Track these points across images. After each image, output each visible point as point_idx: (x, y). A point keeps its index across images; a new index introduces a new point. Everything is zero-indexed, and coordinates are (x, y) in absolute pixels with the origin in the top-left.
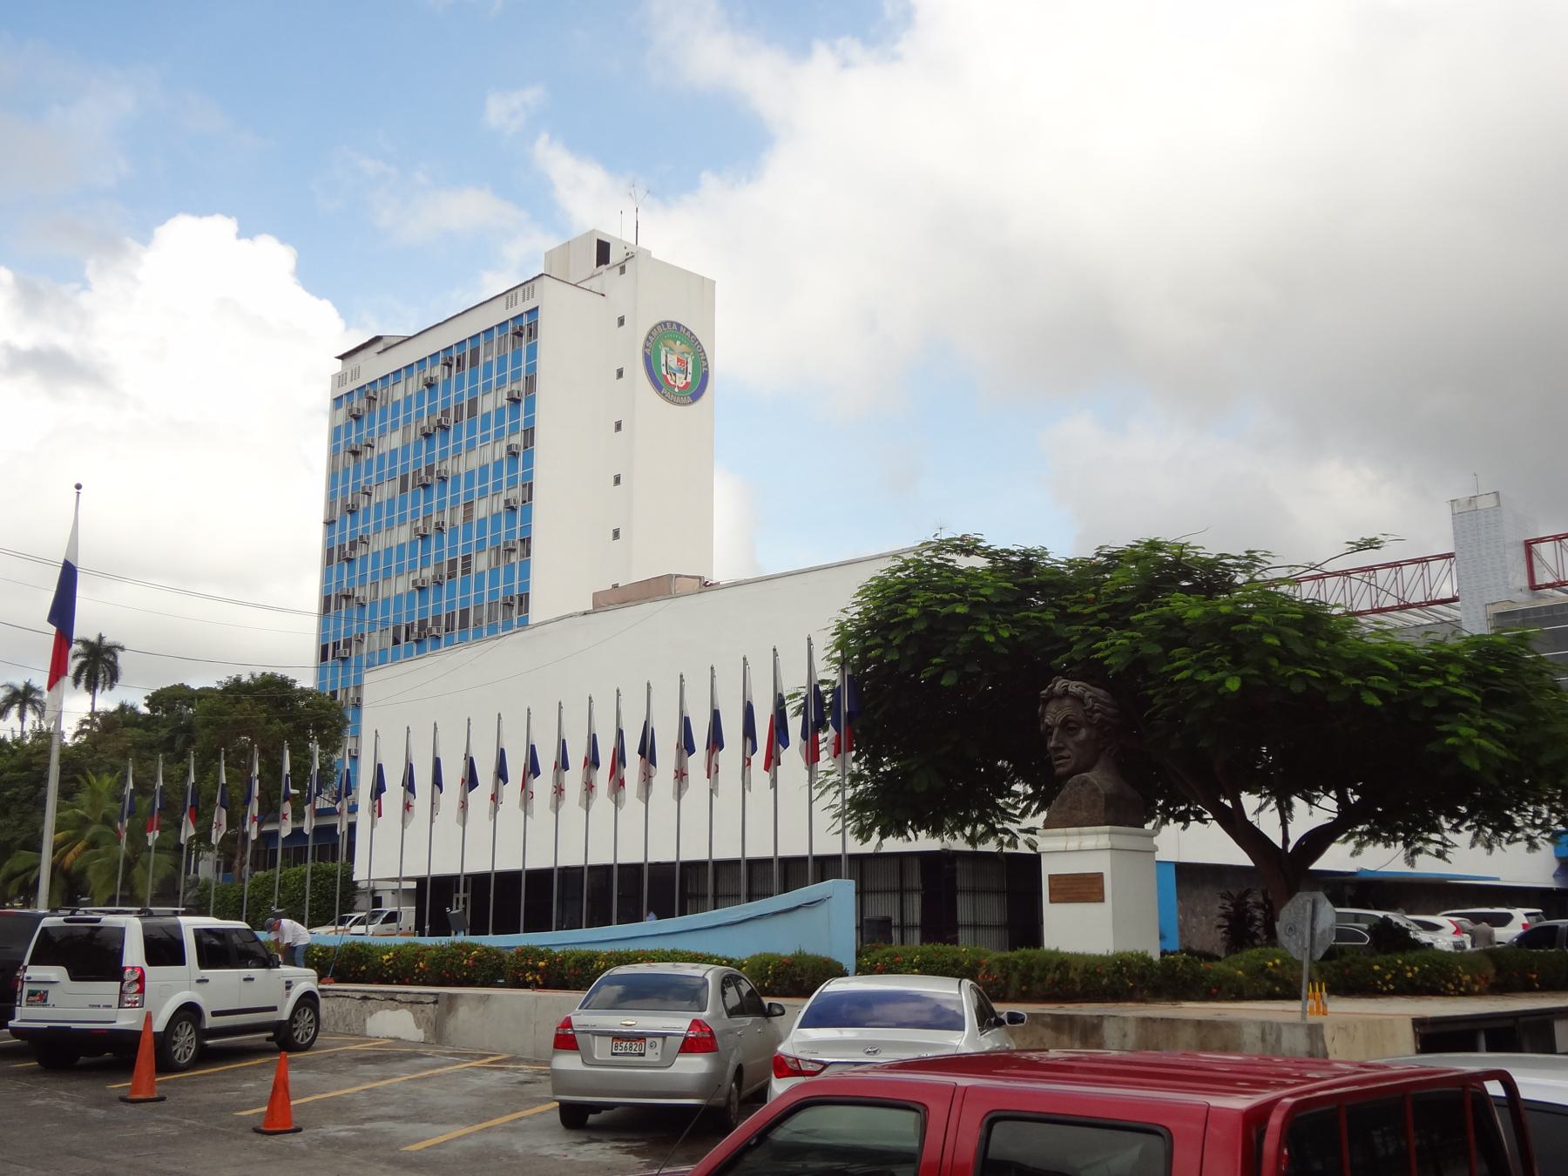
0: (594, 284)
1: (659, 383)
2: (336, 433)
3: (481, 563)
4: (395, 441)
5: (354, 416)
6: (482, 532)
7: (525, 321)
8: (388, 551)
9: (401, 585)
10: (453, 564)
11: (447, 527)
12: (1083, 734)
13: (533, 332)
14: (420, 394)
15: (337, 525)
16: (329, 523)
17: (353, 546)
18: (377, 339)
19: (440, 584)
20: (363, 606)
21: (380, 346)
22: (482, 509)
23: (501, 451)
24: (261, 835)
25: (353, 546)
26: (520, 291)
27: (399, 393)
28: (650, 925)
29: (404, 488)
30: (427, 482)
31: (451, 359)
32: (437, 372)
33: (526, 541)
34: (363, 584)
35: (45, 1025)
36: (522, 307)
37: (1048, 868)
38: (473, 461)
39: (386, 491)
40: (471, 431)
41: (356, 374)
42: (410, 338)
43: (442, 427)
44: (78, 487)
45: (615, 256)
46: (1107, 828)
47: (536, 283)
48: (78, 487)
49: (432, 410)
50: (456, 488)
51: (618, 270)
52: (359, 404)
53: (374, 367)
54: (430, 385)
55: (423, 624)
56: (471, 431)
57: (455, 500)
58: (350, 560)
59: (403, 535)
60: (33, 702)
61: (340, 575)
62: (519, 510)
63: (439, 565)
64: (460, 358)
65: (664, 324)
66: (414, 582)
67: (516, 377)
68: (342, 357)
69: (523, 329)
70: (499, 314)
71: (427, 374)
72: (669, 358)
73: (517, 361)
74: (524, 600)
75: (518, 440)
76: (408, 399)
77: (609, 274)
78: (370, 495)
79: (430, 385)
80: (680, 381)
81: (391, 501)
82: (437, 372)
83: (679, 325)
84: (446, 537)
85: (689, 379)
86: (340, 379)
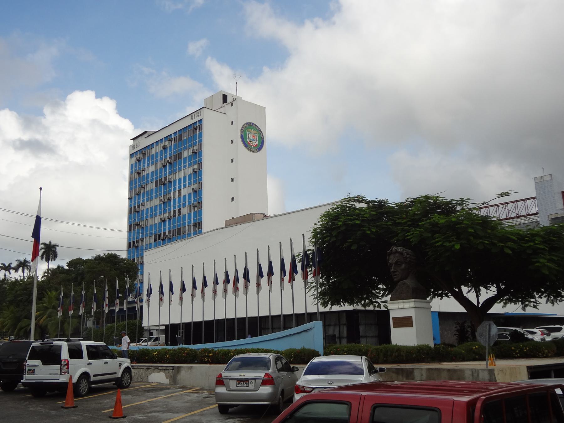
0: (222, 110)
1: (246, 145)
2: (131, 167)
3: (185, 211)
4: (153, 168)
6: (185, 200)
7: (198, 124)
9: (157, 220)
10: (174, 212)
13: (201, 128)
14: (161, 152)
16: (130, 199)
17: (139, 207)
18: (145, 132)
21: (146, 135)
22: (184, 192)
23: (190, 171)
24: (109, 311)
25: (139, 207)
27: (153, 151)
28: (249, 340)
30: (164, 183)
31: (173, 138)
32: (167, 143)
33: (201, 203)
36: (197, 119)
37: (392, 315)
38: (181, 175)
39: (150, 187)
40: (180, 164)
41: (138, 145)
44: (41, 189)
45: (229, 100)
46: (413, 300)
48: (41, 189)
49: (166, 157)
50: (175, 185)
52: (140, 156)
53: (144, 142)
54: (165, 148)
55: (165, 233)
56: (180, 164)
57: (175, 189)
59: (157, 202)
60: (27, 266)
61: (134, 217)
62: (198, 192)
63: (170, 213)
64: (175, 138)
65: (248, 123)
66: (161, 219)
67: (195, 144)
69: (197, 127)
71: (163, 144)
72: (250, 136)
73: (195, 139)
74: (200, 224)
77: (227, 107)
78: (144, 188)
79: (165, 148)
80: (254, 144)
82: (167, 143)
83: (253, 124)
86: (132, 147)
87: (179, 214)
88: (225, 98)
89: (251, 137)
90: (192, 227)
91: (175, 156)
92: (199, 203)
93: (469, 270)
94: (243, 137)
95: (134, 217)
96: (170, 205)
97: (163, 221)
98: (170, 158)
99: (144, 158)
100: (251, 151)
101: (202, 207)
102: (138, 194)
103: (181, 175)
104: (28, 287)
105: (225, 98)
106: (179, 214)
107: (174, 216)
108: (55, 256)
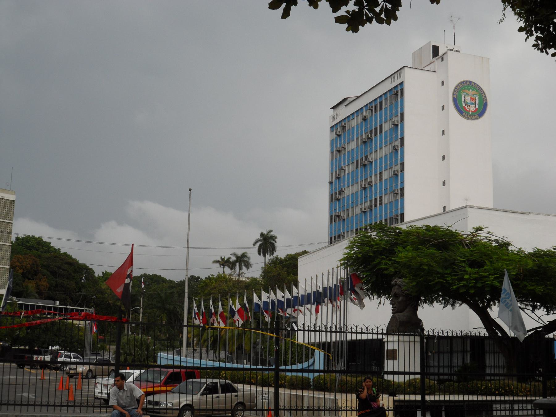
1: (461, 110)
2: (332, 142)
3: (386, 200)
4: (353, 145)
5: (337, 135)
6: (386, 184)
7: (399, 88)
8: (353, 194)
9: (357, 210)
10: (376, 200)
11: (373, 184)
12: (401, 298)
13: (402, 91)
15: (334, 184)
17: (340, 194)
18: (345, 99)
19: (371, 210)
20: (344, 220)
21: (347, 102)
22: (386, 175)
23: (390, 149)
25: (340, 194)
26: (396, 75)
27: (354, 123)
29: (357, 167)
30: (364, 164)
32: (366, 113)
33: (402, 189)
34: (371, 153)
35: (511, 288)
38: (382, 153)
39: (351, 168)
41: (338, 116)
42: (358, 97)
43: (370, 138)
44: (190, 190)
47: (402, 71)
48: (190, 190)
51: (441, 59)
53: (345, 112)
58: (339, 200)
59: (357, 188)
60: (244, 261)
61: (335, 206)
62: (398, 176)
63: (371, 201)
64: (375, 106)
65: (463, 82)
66: (361, 209)
68: (333, 108)
69: (397, 93)
70: (388, 85)
71: (364, 114)
74: (402, 215)
75: (398, 143)
76: (357, 125)
77: (437, 62)
78: (345, 170)
79: (365, 119)
80: (473, 108)
81: (353, 172)
82: (366, 113)
83: (470, 82)
84: (373, 188)
85: (477, 107)
86: (333, 118)
87: (381, 204)
88: (436, 50)
89: (468, 99)
90: (394, 220)
91: (376, 129)
92: (401, 189)
93: (477, 299)
94: (456, 102)
95: (335, 206)
96: (371, 192)
97: (364, 212)
98: (371, 132)
99: (344, 132)
100: (468, 119)
101: (403, 196)
102: (338, 178)
103: (382, 153)
104: (213, 292)
105: (436, 50)
106: (381, 204)
107: (376, 206)
108: (273, 249)
